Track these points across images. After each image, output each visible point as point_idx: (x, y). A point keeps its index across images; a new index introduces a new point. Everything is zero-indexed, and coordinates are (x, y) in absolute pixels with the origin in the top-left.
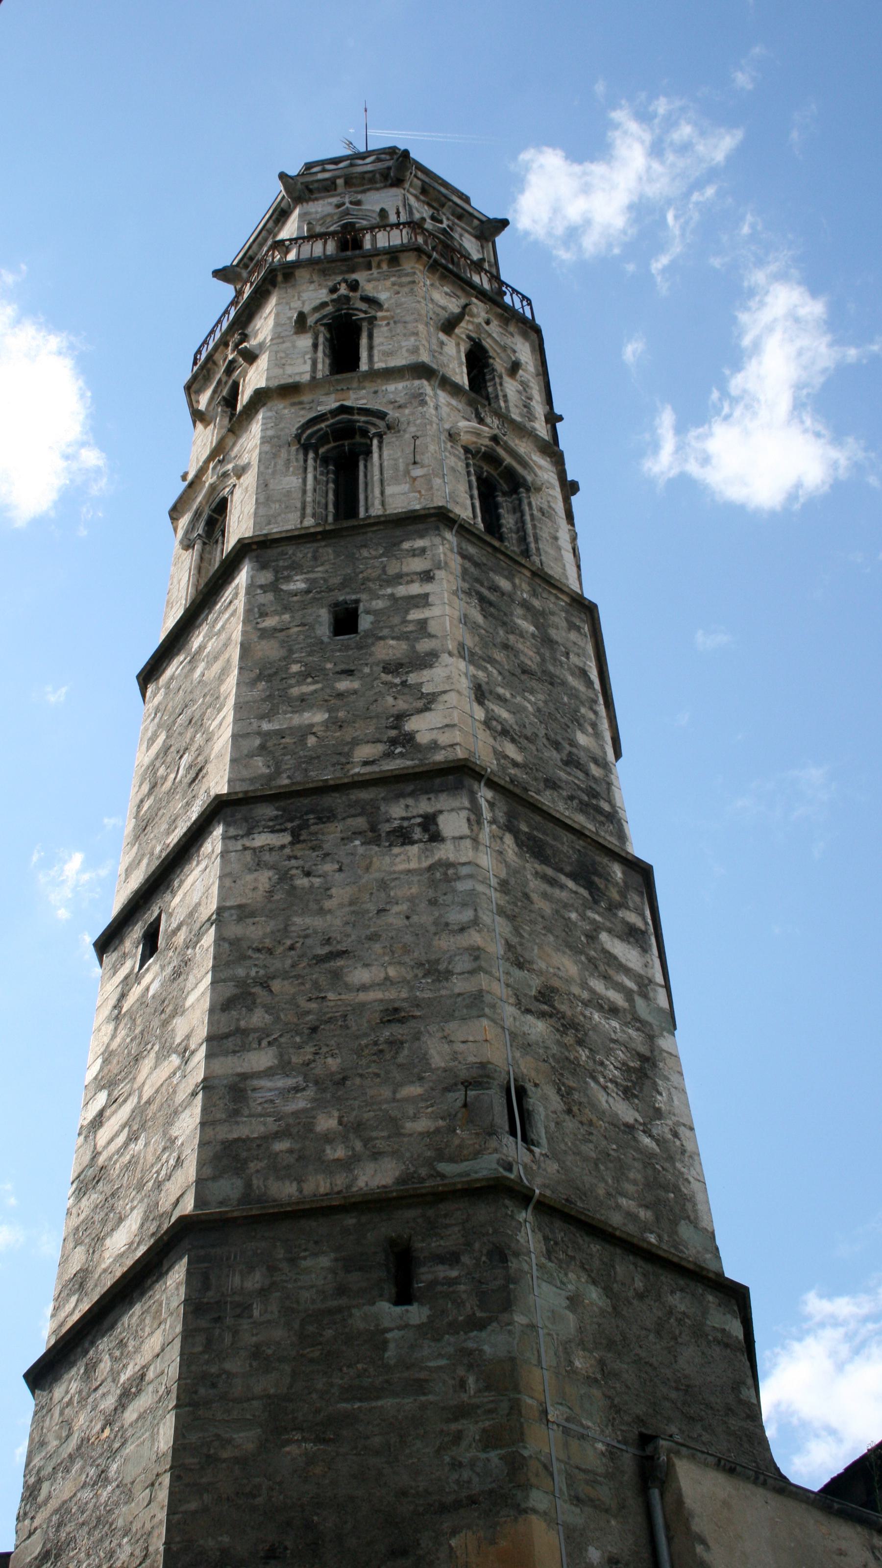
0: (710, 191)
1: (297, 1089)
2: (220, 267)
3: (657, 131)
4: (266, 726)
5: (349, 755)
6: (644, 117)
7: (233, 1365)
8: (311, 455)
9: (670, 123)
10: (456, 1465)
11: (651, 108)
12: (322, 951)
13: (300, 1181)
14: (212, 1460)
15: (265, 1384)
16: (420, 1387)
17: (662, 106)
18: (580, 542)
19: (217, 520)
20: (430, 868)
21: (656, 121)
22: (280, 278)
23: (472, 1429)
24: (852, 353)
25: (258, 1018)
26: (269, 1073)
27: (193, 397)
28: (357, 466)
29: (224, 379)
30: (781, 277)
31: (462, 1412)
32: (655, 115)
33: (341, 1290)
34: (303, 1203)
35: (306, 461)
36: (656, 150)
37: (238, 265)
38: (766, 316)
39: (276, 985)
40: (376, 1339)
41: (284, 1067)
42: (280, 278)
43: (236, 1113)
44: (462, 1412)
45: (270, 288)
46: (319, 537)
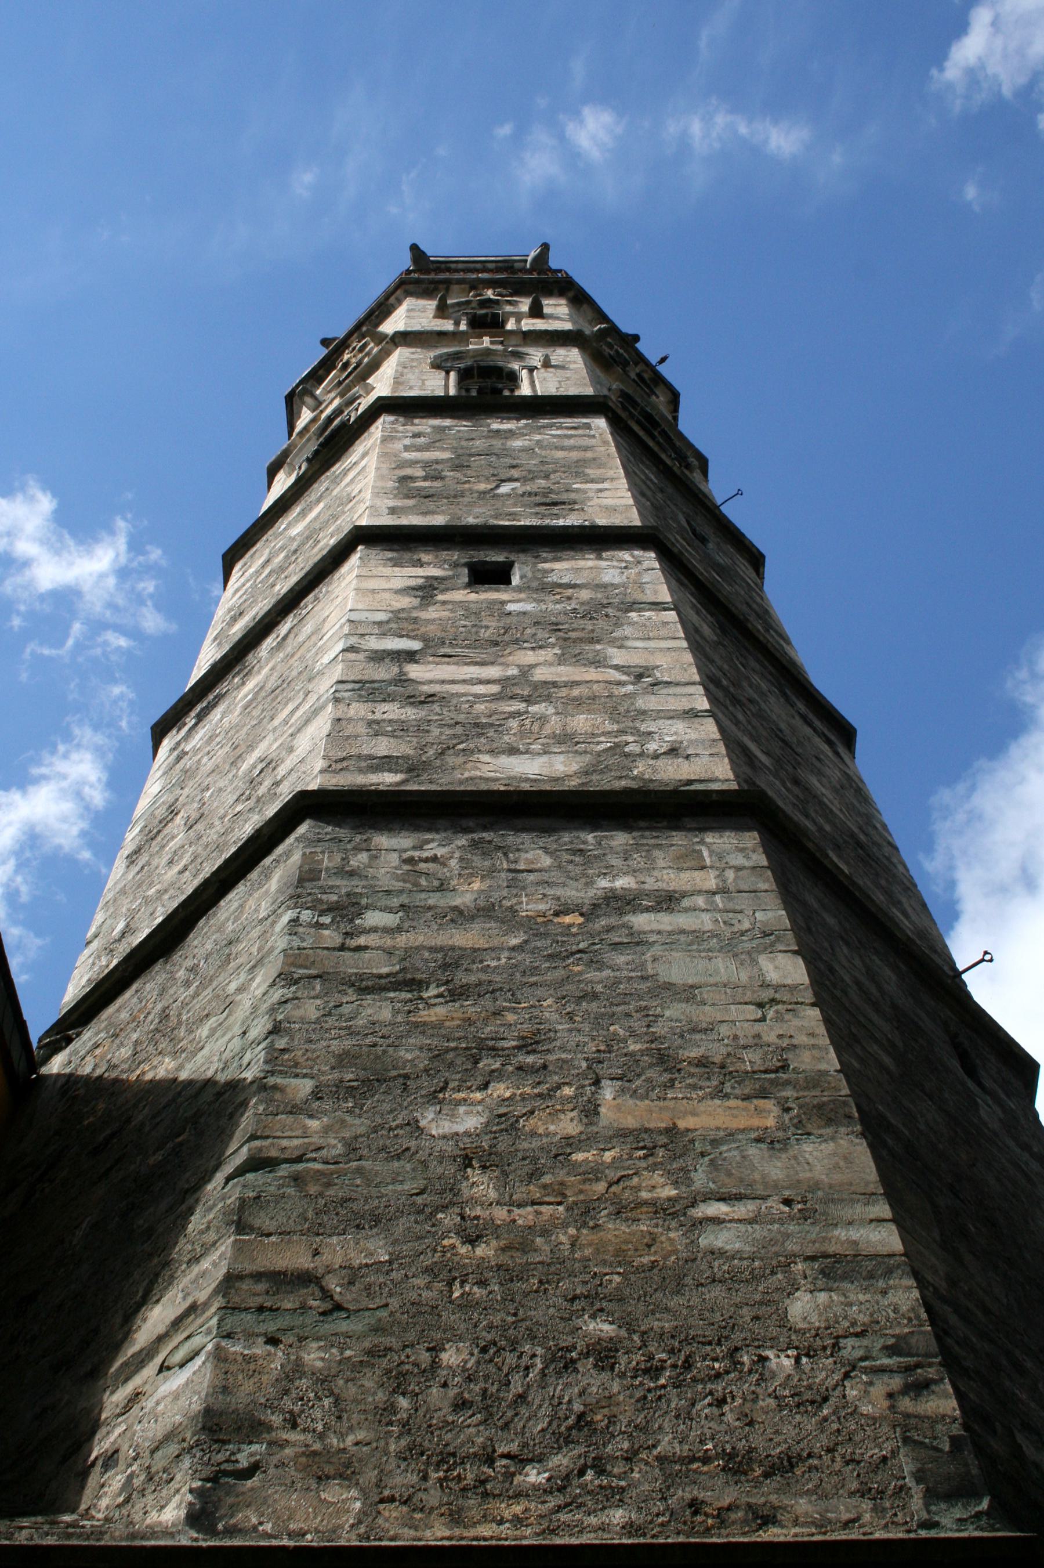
0: (123, 642)
2: (422, 247)
3: (135, 564)
6: (135, 546)
9: (149, 570)
11: (149, 548)
17: (155, 554)
19: (472, 377)
21: (141, 558)
22: (571, 294)
24: (86, 855)
27: (399, 292)
29: (474, 305)
30: (99, 751)
32: (144, 553)
34: (940, 956)
36: (123, 573)
37: (433, 262)
38: (61, 766)
42: (571, 294)
45: (556, 291)
46: (661, 467)
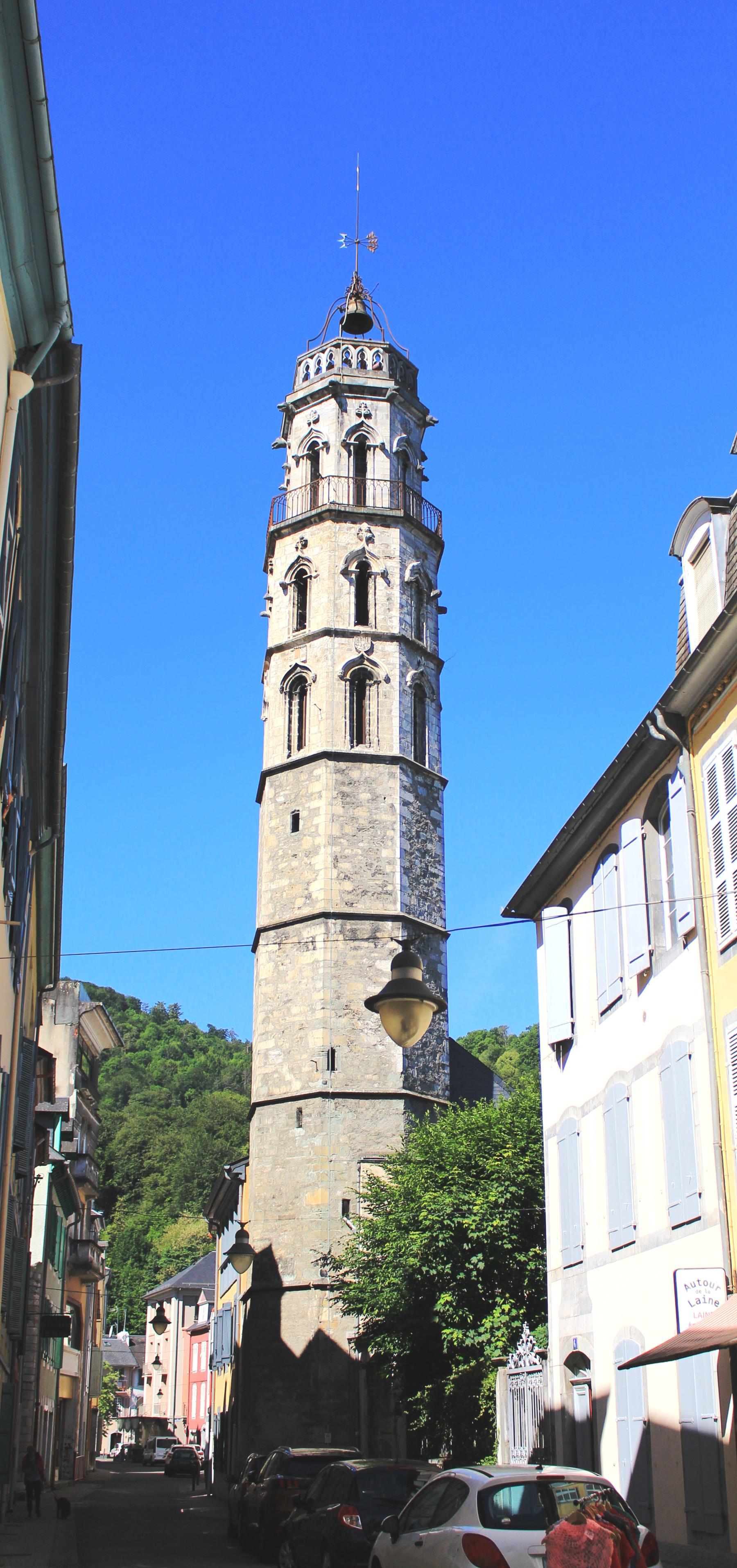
1: (280, 1055)
4: (273, 887)
5: (294, 903)
7: (266, 1146)
8: (399, 417)
10: (308, 1175)
12: (285, 999)
13: (280, 1088)
14: (262, 1172)
15: (272, 1152)
16: (301, 1153)
18: (572, 1263)
20: (313, 963)
23: (311, 1165)
25: (270, 1027)
26: (273, 1049)
28: (215, 1453)
31: (310, 1161)
33: (287, 1125)
35: (290, 704)
39: (275, 1013)
40: (294, 1139)
41: (276, 1047)
43: (265, 1064)
44: (310, 1161)
